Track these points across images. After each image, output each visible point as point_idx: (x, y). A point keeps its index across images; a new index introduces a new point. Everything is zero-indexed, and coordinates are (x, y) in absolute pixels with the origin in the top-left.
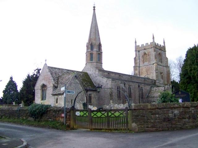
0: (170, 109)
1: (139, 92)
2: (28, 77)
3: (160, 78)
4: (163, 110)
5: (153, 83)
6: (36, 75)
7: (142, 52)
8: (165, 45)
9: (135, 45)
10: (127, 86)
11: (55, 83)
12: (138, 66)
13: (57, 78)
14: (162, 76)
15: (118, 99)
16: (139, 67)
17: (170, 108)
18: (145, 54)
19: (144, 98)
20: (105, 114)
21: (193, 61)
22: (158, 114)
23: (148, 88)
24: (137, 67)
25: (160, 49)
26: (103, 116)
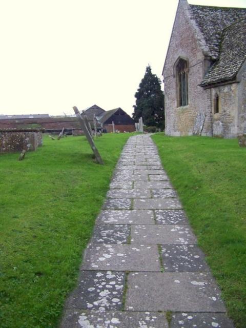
11: (211, 50)
13: (219, 34)
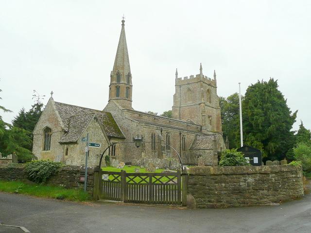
0: (241, 176)
2: (22, 114)
3: (207, 122)
4: (231, 176)
5: (199, 129)
6: (35, 113)
8: (217, 79)
11: (65, 126)
14: (211, 120)
16: (180, 107)
17: (240, 174)
19: (187, 151)
20: (156, 180)
21: (255, 102)
22: (225, 182)
25: (209, 85)
26: (143, 182)
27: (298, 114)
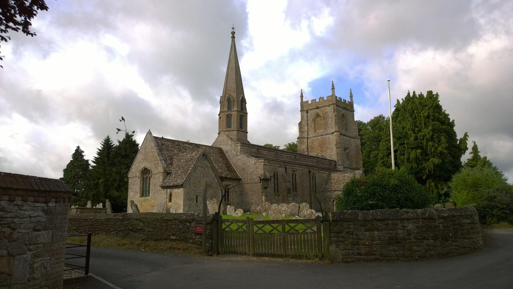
1: (310, 182)
7: (312, 113)
9: (300, 101)
10: (290, 171)
12: (306, 136)
14: (348, 154)
15: (275, 195)
16: (307, 138)
18: (318, 115)
22: (378, 230)
23: (325, 174)
24: (304, 138)
25: (345, 108)
27: (477, 143)
